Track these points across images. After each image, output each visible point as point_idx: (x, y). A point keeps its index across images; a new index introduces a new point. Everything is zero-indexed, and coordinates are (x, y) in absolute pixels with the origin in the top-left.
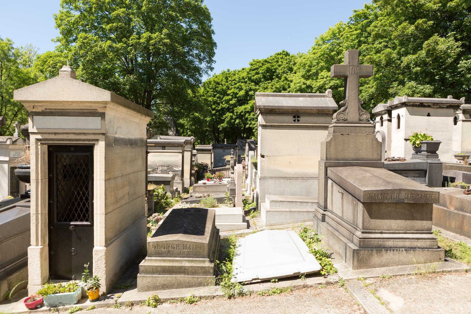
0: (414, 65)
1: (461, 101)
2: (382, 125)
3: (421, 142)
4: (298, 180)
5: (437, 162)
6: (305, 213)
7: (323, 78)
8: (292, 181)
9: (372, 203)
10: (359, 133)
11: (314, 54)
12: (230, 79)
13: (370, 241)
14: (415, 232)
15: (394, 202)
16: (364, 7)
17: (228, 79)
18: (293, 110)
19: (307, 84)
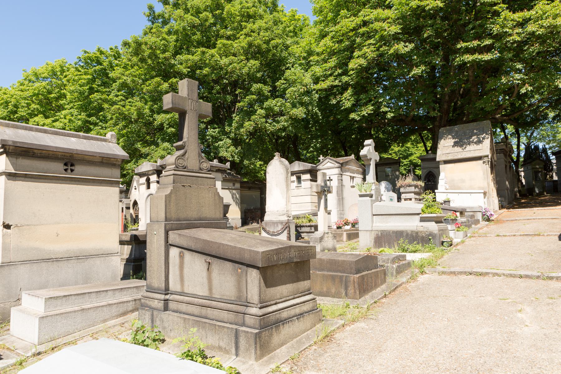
0: (167, 125)
1: (227, 166)
2: (148, 187)
4: (70, 261)
6: (105, 309)
8: (60, 264)
9: (269, 266)
10: (201, 185)
14: (300, 295)
16: (96, 49)
18: (63, 154)
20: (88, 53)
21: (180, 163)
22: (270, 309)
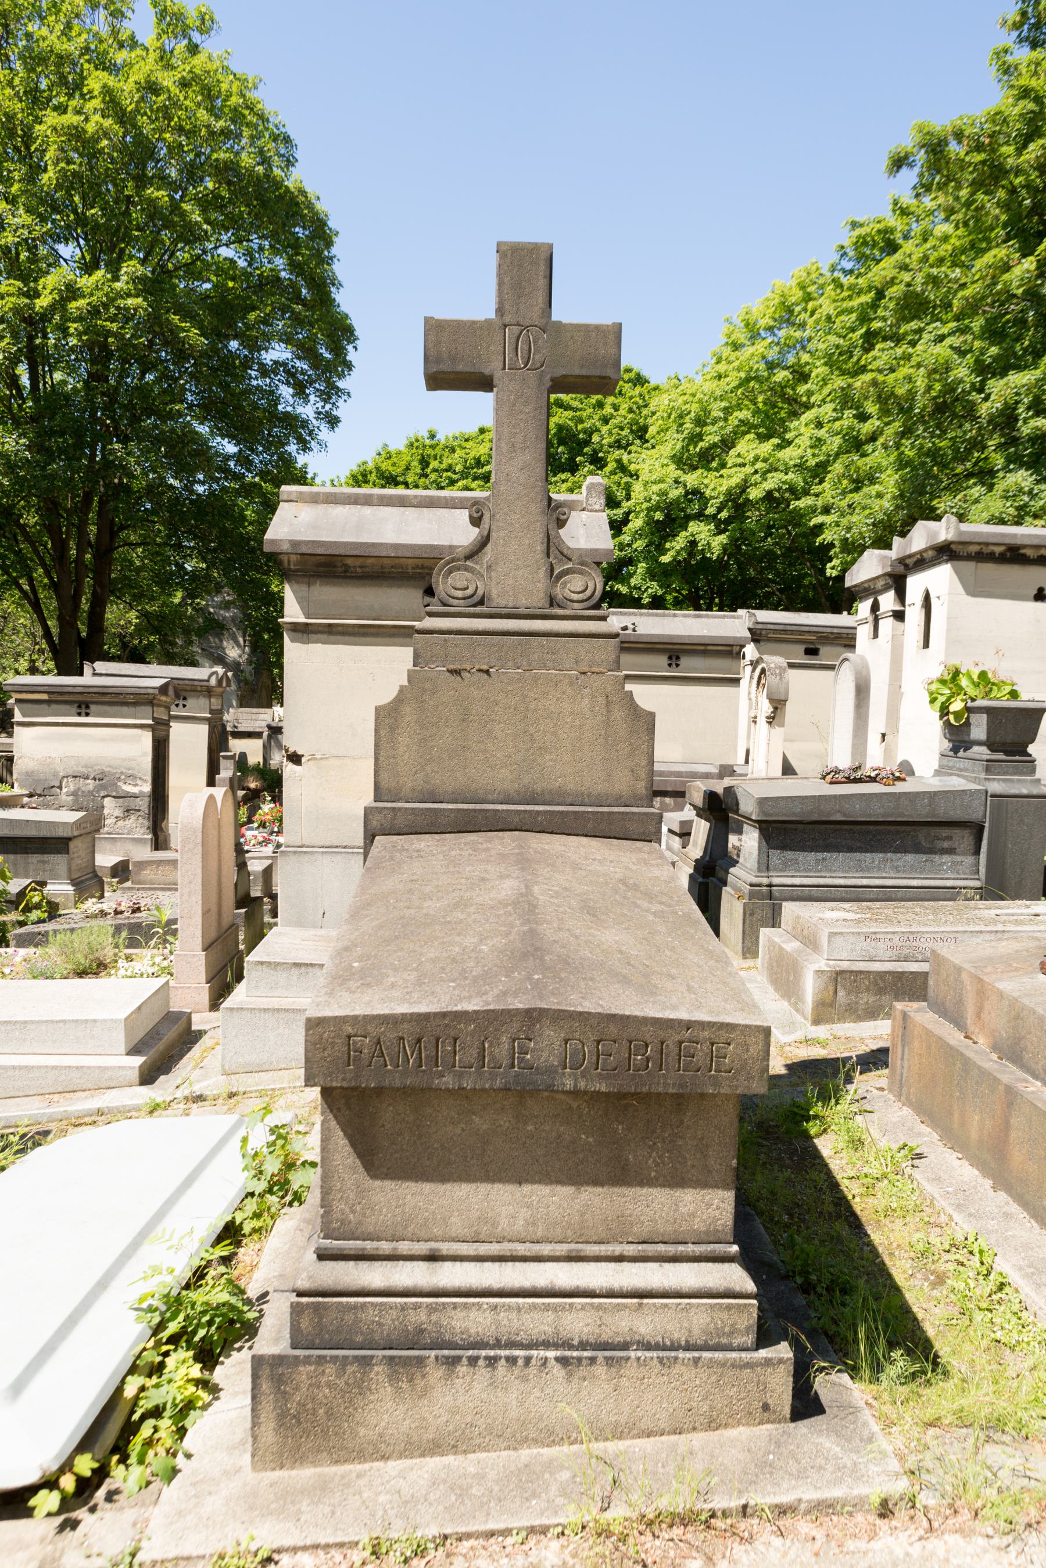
0: (1029, 409)
3: (970, 704)
5: (1025, 791)
7: (744, 465)
10: (544, 667)
11: (719, 377)
12: (434, 464)
13: (355, 1307)
14: (631, 1250)
15: (498, 1084)
17: (428, 465)
18: (420, 562)
19: (689, 486)
20: (861, 225)
21: (458, 585)
22: (374, 1275)
